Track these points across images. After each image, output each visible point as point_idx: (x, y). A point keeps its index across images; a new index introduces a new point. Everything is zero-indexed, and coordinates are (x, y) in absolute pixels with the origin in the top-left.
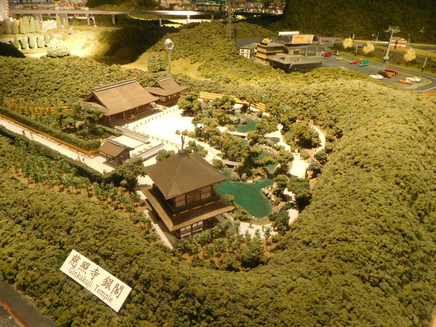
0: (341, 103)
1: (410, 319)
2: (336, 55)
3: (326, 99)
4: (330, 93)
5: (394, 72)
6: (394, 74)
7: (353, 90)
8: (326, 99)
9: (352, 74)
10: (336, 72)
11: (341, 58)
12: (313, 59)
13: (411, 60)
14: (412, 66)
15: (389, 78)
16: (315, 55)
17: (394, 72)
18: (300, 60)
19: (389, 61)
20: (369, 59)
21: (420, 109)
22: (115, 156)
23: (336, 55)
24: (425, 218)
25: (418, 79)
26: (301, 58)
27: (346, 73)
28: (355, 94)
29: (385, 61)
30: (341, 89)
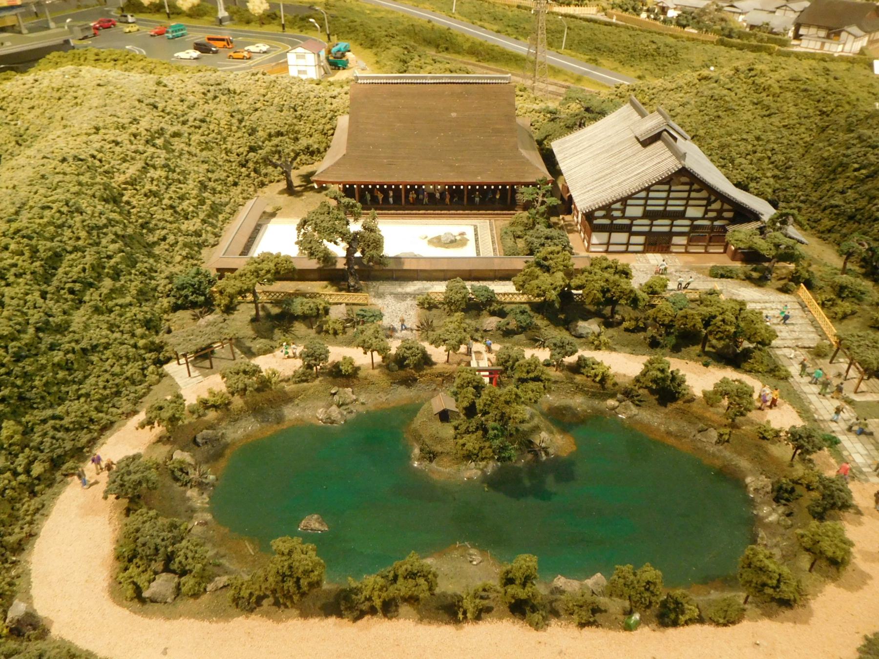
0: (38, 122)
1: (159, 381)
2: (127, 22)
3: (10, 117)
4: (12, 105)
5: (223, 40)
6: (225, 43)
7: (53, 88)
8: (10, 117)
9: (114, 57)
10: (82, 59)
11: (134, 28)
12: (45, 37)
13: (261, 12)
14: (270, 23)
15: (216, 52)
16: (48, 28)
17: (223, 40)
18: (8, 44)
19: (231, 19)
20: (194, 22)
21: (152, 101)
22: (273, 220)
23: (127, 22)
24: (677, 162)
25: (263, 47)
26: (8, 39)
27: (102, 56)
28: (57, 95)
29: (221, 21)
30: (35, 90)
